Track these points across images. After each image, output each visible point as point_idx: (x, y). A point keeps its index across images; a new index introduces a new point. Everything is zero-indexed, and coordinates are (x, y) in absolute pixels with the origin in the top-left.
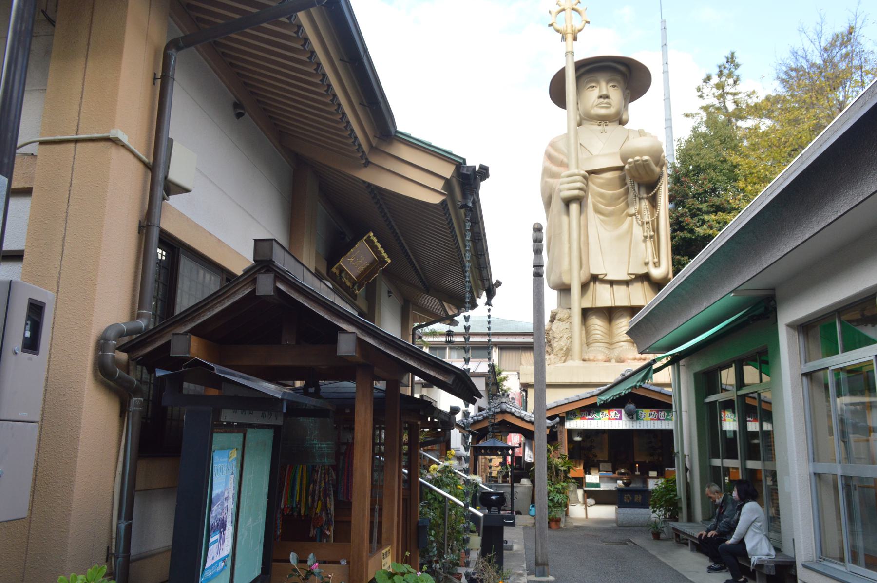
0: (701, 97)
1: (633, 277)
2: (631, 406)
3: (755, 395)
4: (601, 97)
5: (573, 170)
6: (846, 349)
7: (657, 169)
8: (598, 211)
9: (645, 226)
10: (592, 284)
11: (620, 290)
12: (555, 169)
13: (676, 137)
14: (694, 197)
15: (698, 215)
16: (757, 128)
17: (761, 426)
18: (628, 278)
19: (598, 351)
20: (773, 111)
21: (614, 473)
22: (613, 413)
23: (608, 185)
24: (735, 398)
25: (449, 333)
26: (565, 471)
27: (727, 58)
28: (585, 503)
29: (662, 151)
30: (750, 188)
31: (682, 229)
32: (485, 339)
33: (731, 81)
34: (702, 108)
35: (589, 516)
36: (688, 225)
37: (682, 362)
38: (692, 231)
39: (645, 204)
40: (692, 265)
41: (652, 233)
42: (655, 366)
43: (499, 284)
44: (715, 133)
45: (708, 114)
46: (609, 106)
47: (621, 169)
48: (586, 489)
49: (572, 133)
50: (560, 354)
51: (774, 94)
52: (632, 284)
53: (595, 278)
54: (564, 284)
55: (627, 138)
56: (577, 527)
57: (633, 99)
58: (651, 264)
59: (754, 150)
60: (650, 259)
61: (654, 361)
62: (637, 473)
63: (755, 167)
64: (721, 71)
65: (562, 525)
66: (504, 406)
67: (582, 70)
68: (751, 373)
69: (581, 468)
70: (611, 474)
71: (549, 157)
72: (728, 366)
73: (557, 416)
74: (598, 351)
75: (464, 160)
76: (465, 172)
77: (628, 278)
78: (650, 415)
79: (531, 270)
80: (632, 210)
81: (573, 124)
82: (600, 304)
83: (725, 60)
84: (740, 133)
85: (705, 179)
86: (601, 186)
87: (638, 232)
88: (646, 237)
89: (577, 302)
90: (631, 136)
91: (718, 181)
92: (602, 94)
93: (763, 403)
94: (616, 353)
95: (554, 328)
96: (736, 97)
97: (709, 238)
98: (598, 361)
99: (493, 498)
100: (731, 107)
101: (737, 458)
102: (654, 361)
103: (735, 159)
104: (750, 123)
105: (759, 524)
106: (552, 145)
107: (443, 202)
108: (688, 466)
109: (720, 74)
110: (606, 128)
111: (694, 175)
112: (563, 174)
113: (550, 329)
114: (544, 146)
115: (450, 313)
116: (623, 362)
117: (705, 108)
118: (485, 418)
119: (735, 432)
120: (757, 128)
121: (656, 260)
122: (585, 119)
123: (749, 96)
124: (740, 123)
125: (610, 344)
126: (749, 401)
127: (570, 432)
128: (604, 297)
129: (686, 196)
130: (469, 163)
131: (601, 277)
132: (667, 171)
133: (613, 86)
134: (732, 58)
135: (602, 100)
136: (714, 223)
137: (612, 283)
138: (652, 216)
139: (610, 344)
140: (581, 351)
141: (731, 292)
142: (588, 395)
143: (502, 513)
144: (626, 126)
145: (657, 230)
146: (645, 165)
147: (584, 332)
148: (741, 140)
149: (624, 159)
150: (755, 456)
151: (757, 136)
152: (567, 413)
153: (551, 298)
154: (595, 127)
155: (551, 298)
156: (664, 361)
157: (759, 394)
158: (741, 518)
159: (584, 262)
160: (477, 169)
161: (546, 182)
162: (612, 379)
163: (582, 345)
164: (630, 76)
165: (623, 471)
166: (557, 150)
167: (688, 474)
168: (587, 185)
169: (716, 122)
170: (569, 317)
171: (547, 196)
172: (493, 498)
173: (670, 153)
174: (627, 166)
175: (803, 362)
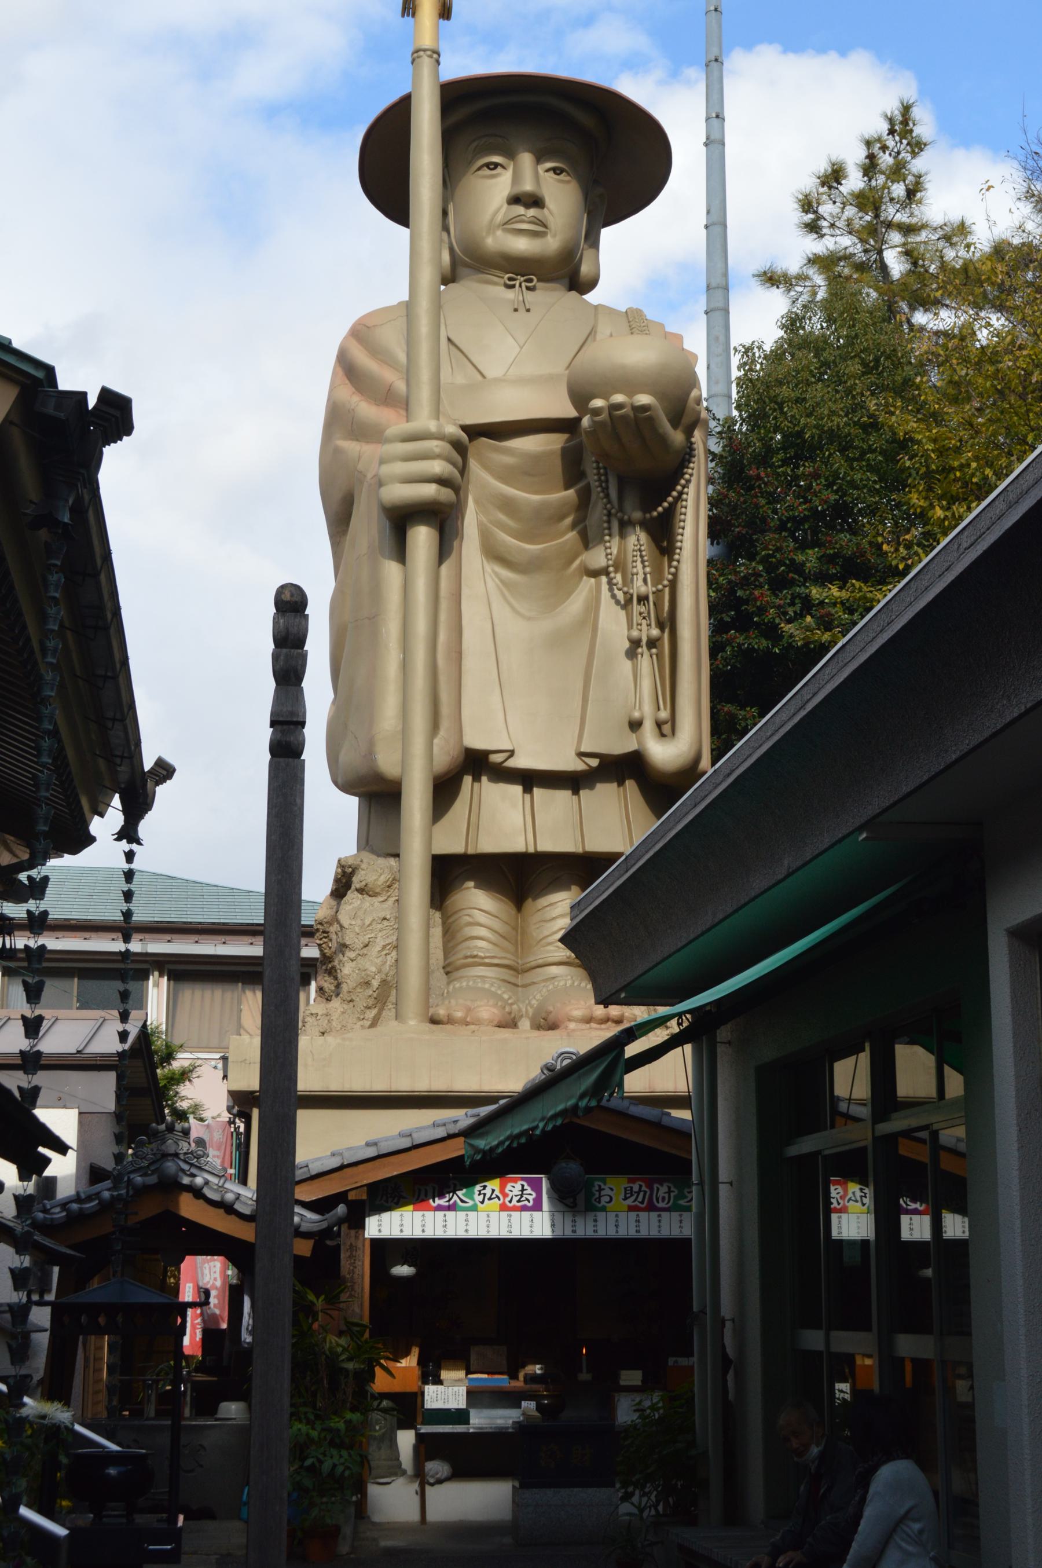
0: (813, 228)
1: (594, 763)
2: (572, 1168)
3: (924, 1134)
4: (515, 200)
5: (424, 420)
7: (677, 437)
8: (493, 553)
9: (636, 608)
10: (468, 780)
11: (554, 803)
12: (367, 410)
13: (739, 337)
14: (782, 527)
15: (792, 583)
16: (966, 334)
17: (937, 1226)
18: (578, 765)
19: (481, 991)
20: (1012, 291)
21: (514, 1376)
23: (527, 472)
24: (868, 1142)
26: (357, 1374)
27: (891, 120)
28: (420, 1475)
29: (693, 382)
30: (939, 513)
31: (743, 623)
32: (113, 945)
33: (899, 190)
34: (814, 260)
35: (432, 1516)
36: (762, 610)
37: (724, 1033)
38: (772, 632)
39: (638, 540)
40: (763, 732)
41: (655, 632)
42: (632, 1050)
43: (164, 771)
44: (851, 340)
45: (835, 281)
48: (425, 1429)
49: (424, 304)
50: (362, 998)
51: (1016, 241)
52: (591, 787)
53: (477, 764)
55: (592, 333)
56: (392, 1553)
57: (615, 217)
58: (648, 726)
59: (955, 401)
60: (647, 711)
61: (631, 1034)
62: (584, 1376)
63: (958, 450)
64: (871, 157)
65: (344, 1548)
67: (462, 112)
68: (915, 1069)
69: (410, 1362)
70: (502, 1381)
71: (347, 368)
72: (854, 1050)
73: (340, 1197)
74: (481, 991)
75: (50, 371)
76: (50, 410)
77: (577, 765)
78: (628, 1193)
80: (597, 558)
81: (427, 276)
82: (488, 845)
83: (885, 127)
84: (920, 348)
85: (816, 476)
86: (506, 475)
87: (614, 626)
88: (635, 643)
89: (420, 837)
90: (604, 329)
91: (853, 484)
92: (513, 193)
93: (943, 1155)
94: (535, 997)
95: (344, 918)
96: (913, 239)
97: (814, 652)
98: (477, 1022)
99: (112, 1471)
100: (896, 264)
101: (868, 1328)
102: (631, 1034)
103: (903, 422)
104: (946, 319)
105: (916, 1526)
106: (361, 333)
108: (730, 1351)
109: (870, 167)
110: (529, 296)
111: (785, 462)
112: (392, 431)
113: (335, 919)
114: (333, 336)
116: (553, 1026)
117: (824, 263)
118: (105, 1207)
119: (865, 1243)
120: (966, 334)
121: (664, 714)
122: (466, 263)
123: (947, 238)
124: (920, 318)
125: (519, 971)
126: (906, 1149)
127: (386, 1250)
128: (504, 820)
129: (758, 524)
130: (65, 383)
132: (706, 444)
133: (556, 171)
134: (905, 122)
135: (520, 210)
136: (839, 612)
137: (530, 780)
138: (658, 578)
139: (519, 971)
140: (427, 990)
141: (860, 829)
142: (441, 1133)
143: (140, 1519)
144: (592, 297)
145: (669, 622)
147: (437, 932)
148: (921, 368)
149: (580, 397)
150: (919, 1326)
151: (965, 360)
153: (331, 820)
154: (497, 291)
155: (331, 820)
156: (674, 1027)
157: (935, 1135)
158: (868, 1512)
159: (445, 710)
160: (92, 402)
161: (338, 451)
162: (515, 1083)
163: (427, 972)
165: (538, 1369)
166: (375, 350)
167: (730, 1377)
168: (463, 470)
169: (853, 308)
170: (395, 882)
172: (112, 1471)
173: (720, 388)
174: (586, 421)
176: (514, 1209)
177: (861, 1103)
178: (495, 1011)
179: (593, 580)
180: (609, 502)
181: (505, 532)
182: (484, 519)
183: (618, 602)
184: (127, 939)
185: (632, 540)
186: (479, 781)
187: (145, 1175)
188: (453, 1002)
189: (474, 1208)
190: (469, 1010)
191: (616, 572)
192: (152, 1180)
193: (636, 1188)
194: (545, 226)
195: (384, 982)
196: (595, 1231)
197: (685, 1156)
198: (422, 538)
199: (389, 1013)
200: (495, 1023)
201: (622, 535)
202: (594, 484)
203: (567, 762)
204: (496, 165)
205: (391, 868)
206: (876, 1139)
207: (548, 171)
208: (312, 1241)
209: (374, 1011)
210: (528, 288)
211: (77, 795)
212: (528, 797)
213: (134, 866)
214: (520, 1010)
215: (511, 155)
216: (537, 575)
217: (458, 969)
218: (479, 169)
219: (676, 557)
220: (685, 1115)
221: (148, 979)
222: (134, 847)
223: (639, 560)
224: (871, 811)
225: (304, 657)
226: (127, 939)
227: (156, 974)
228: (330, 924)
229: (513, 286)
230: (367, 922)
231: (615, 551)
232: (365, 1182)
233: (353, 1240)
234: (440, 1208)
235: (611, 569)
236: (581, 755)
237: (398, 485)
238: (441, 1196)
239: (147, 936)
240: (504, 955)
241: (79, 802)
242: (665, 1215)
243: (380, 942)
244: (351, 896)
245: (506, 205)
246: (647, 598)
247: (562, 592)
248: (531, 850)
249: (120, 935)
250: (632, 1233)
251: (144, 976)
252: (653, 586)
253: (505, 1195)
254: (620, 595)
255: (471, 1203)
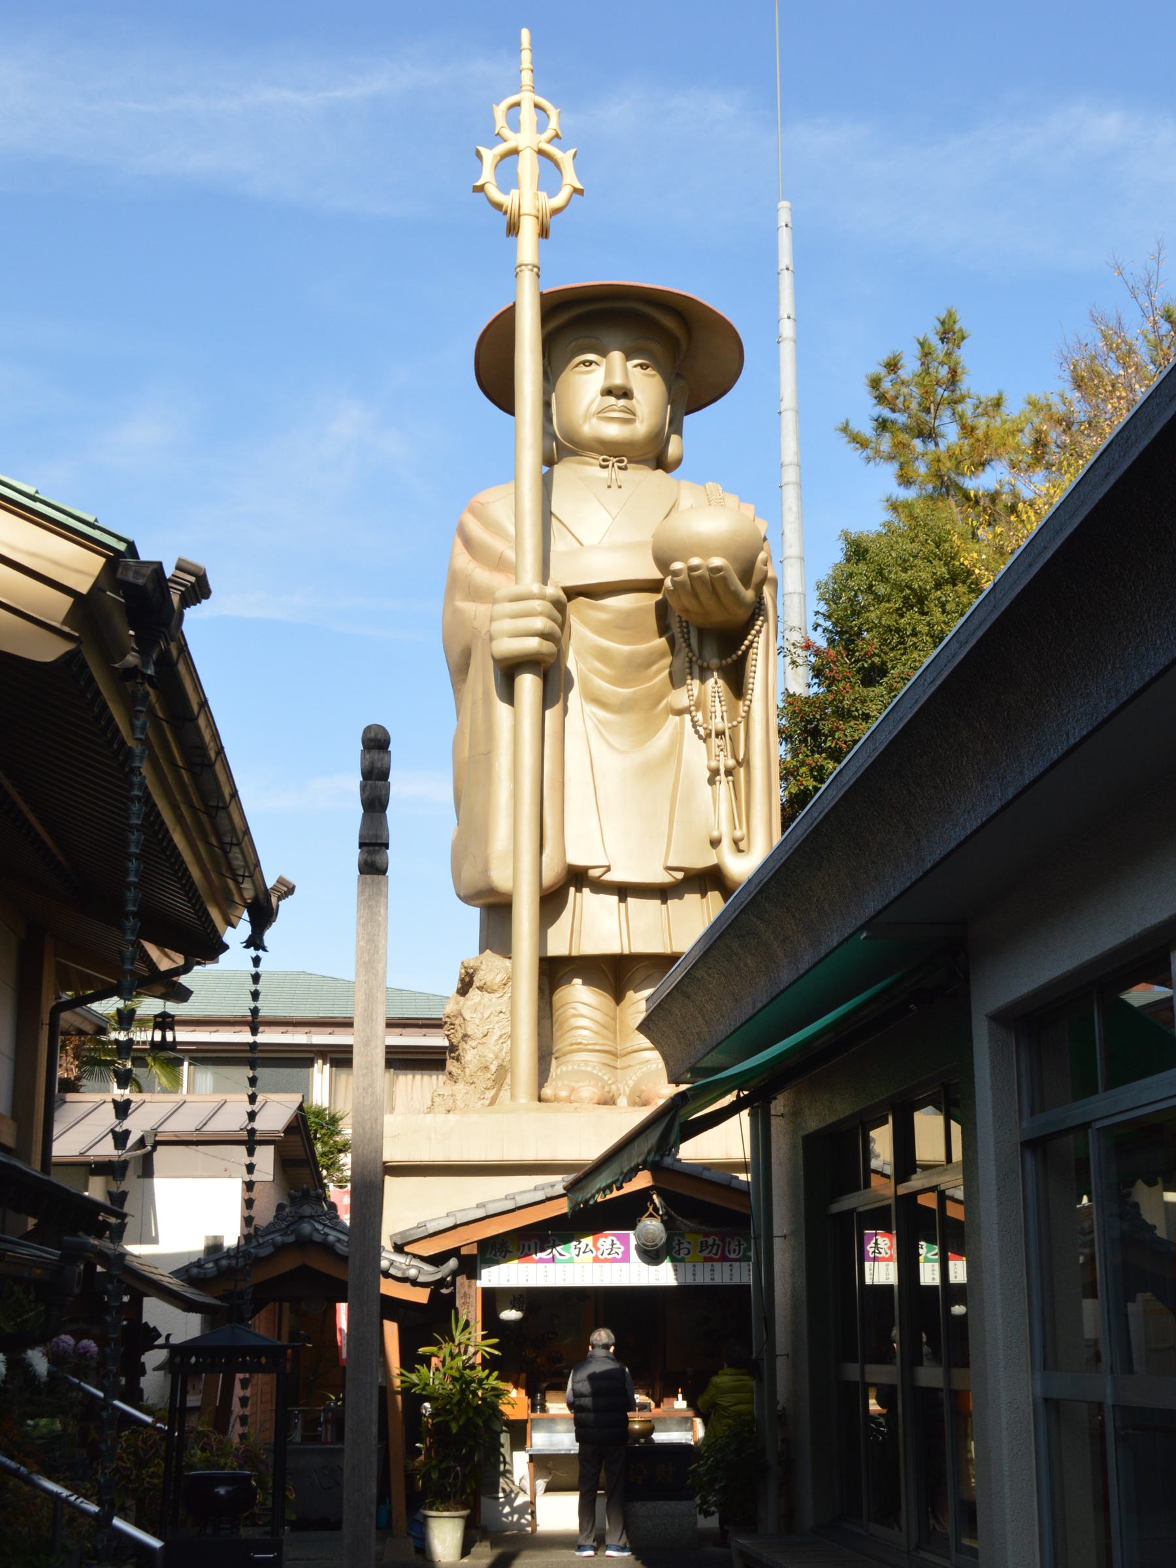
1: (680, 875)
4: (608, 392)
6: (1114, 1082)
7: (749, 594)
10: (572, 890)
22: (607, 1241)
23: (623, 626)
24: (891, 1201)
25: (164, 1022)
32: (243, 1036)
39: (715, 685)
43: (286, 889)
46: (630, 417)
47: (653, 586)
53: (577, 877)
54: (492, 891)
57: (696, 405)
58: (726, 844)
60: (725, 831)
66: (306, 1228)
73: (454, 1252)
75: (131, 546)
76: (130, 577)
77: (665, 878)
79: (353, 854)
80: (680, 698)
86: (602, 629)
87: (697, 756)
88: (715, 772)
92: (610, 388)
107: (67, 659)
112: (500, 594)
115: (164, 965)
125: (614, 1055)
127: (493, 1299)
128: (596, 926)
131: (594, 873)
133: (641, 365)
135: (612, 400)
137: (623, 891)
138: (732, 713)
142: (540, 1196)
146: (714, 582)
149: (663, 563)
152: (483, 1244)
161: (456, 612)
164: (690, 349)
170: (509, 981)
171: (457, 650)
174: (668, 582)
175: (1026, 1110)
176: (606, 1260)
177: (744, 1167)
178: (595, 1090)
179: (677, 718)
180: (691, 650)
181: (602, 678)
182: (584, 668)
183: (700, 737)
184: (254, 1032)
185: (711, 682)
186: (581, 891)
187: (285, 1234)
188: (560, 1083)
189: (571, 1261)
190: (572, 1090)
191: (697, 710)
192: (291, 1239)
193: (710, 1241)
194: (634, 414)
195: (501, 1067)
196: (712, 1279)
197: (745, 1211)
198: (528, 684)
199: (505, 1094)
200: (595, 1100)
201: (703, 680)
202: (678, 635)
203: (658, 876)
204: (591, 363)
205: (506, 968)
206: (898, 1198)
207: (635, 366)
208: (429, 1290)
209: (493, 1092)
210: (620, 468)
211: (206, 909)
212: (622, 905)
213: (259, 970)
214: (618, 1089)
215: (603, 353)
216: (645, 713)
217: (565, 1054)
218: (577, 366)
219: (749, 697)
220: (743, 1177)
221: (312, 1066)
222: (261, 953)
223: (717, 700)
224: (869, 912)
225: (387, 788)
226: (254, 1032)
227: (320, 1062)
228: (456, 1017)
229: (607, 467)
230: (486, 1016)
231: (696, 692)
232: (476, 1239)
233: (466, 1289)
234: (541, 1261)
235: (693, 708)
236: (669, 869)
237: (507, 639)
238: (543, 1250)
239: (313, 1029)
240: (603, 1042)
241: (208, 915)
242: (736, 1265)
243: (497, 1033)
244: (474, 993)
245: (600, 397)
246: (723, 733)
247: (650, 728)
248: (626, 951)
249: (248, 1029)
250: (708, 1281)
251: (310, 1063)
252: (729, 721)
253: (598, 1249)
254: (702, 732)
255: (568, 1256)
